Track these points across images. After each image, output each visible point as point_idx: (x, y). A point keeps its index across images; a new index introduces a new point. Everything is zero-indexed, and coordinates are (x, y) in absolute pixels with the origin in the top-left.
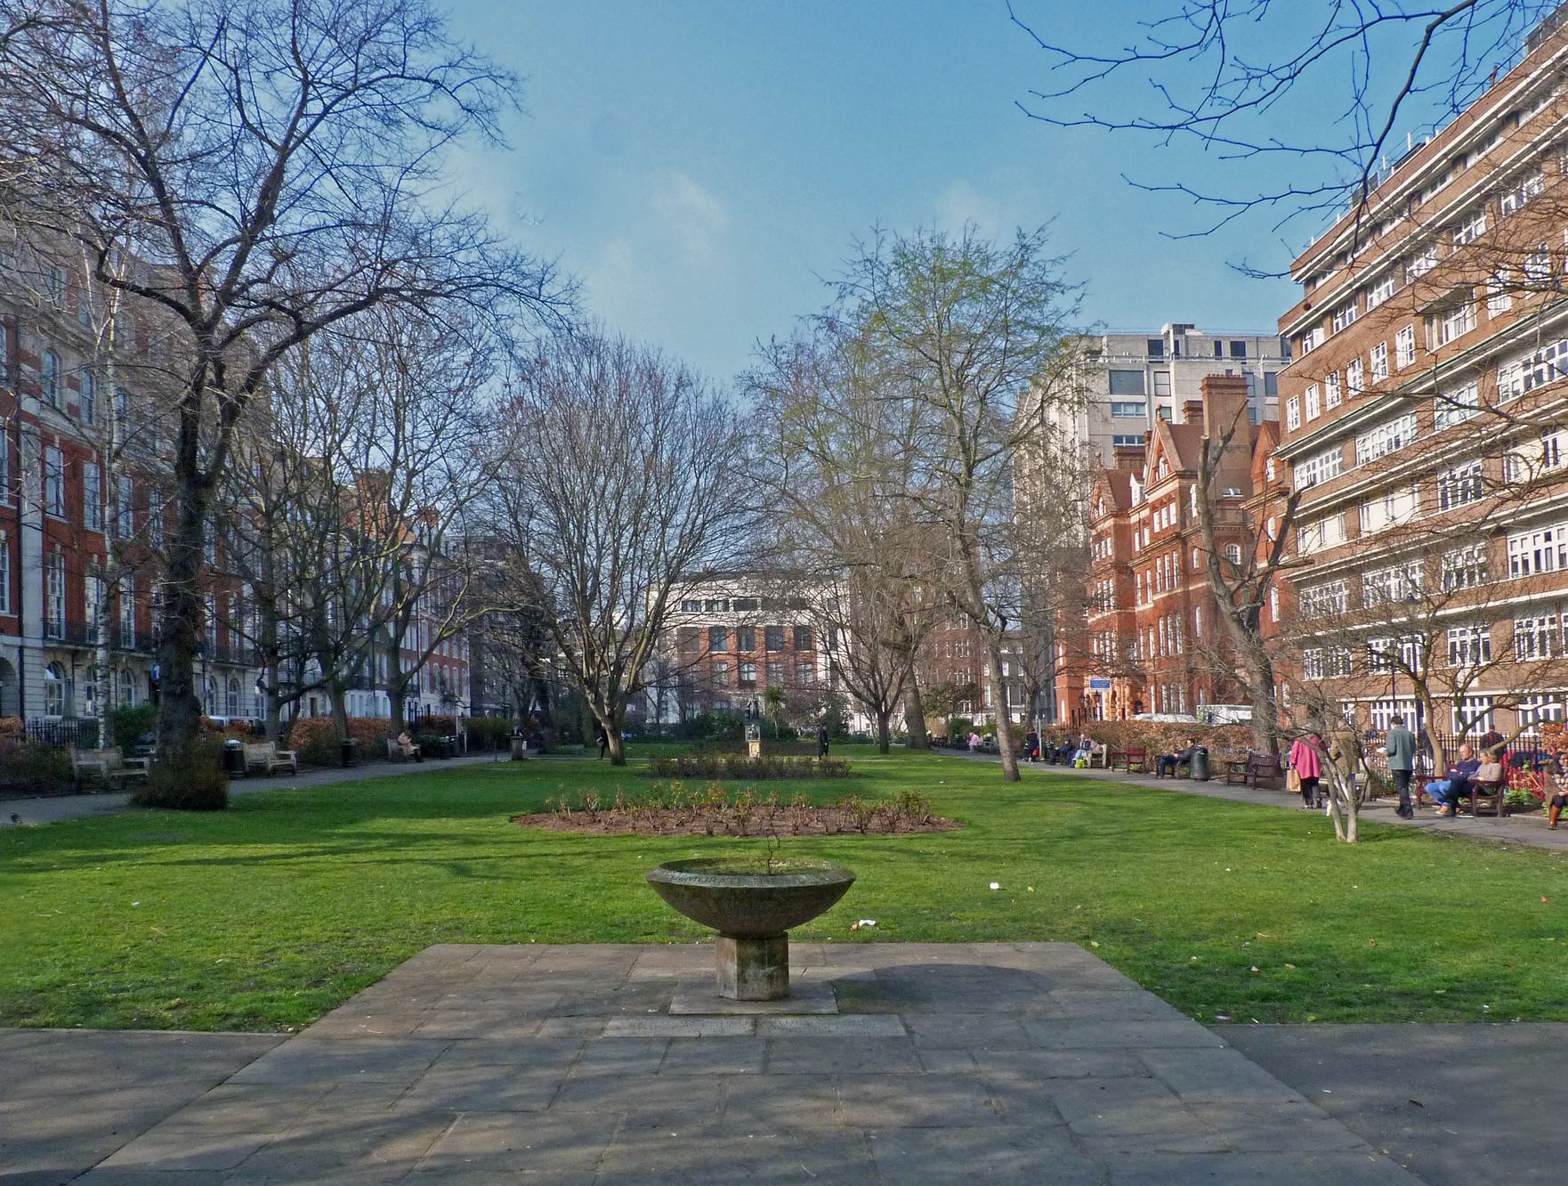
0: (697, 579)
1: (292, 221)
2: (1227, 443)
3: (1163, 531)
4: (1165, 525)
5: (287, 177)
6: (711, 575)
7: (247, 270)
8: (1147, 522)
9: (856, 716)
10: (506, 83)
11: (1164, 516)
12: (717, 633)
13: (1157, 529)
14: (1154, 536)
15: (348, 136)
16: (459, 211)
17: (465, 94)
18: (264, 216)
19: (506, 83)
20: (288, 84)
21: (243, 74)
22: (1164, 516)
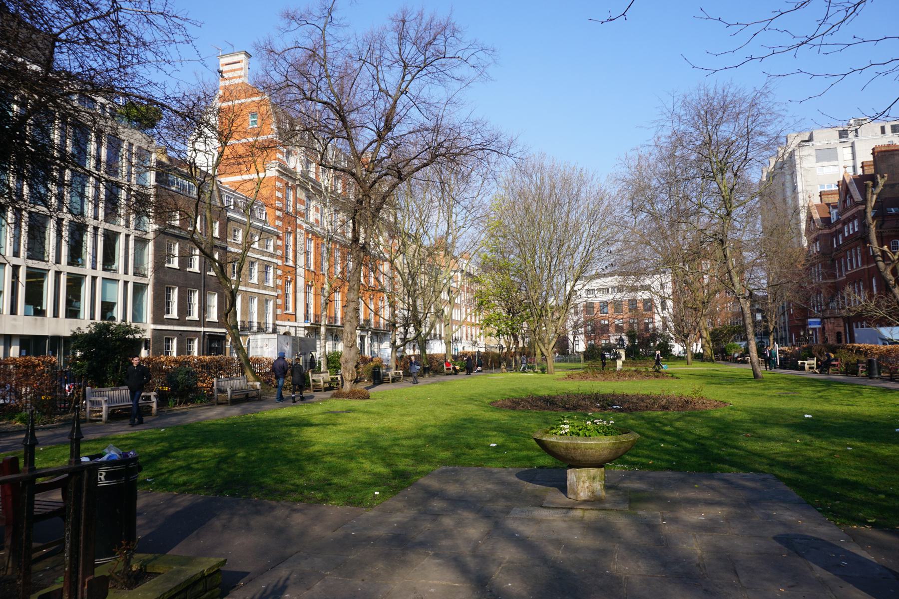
0: (592, 278)
1: (400, 130)
2: (799, 392)
3: (850, 235)
4: (851, 232)
5: (398, 110)
6: (598, 276)
7: (576, 288)
8: (841, 231)
9: (676, 345)
10: (490, 52)
11: (851, 227)
12: (605, 304)
13: (846, 235)
14: (844, 238)
15: (426, 88)
16: (473, 118)
17: (473, 61)
18: (388, 127)
19: (490, 52)
20: (398, 70)
21: (379, 68)
22: (851, 227)
